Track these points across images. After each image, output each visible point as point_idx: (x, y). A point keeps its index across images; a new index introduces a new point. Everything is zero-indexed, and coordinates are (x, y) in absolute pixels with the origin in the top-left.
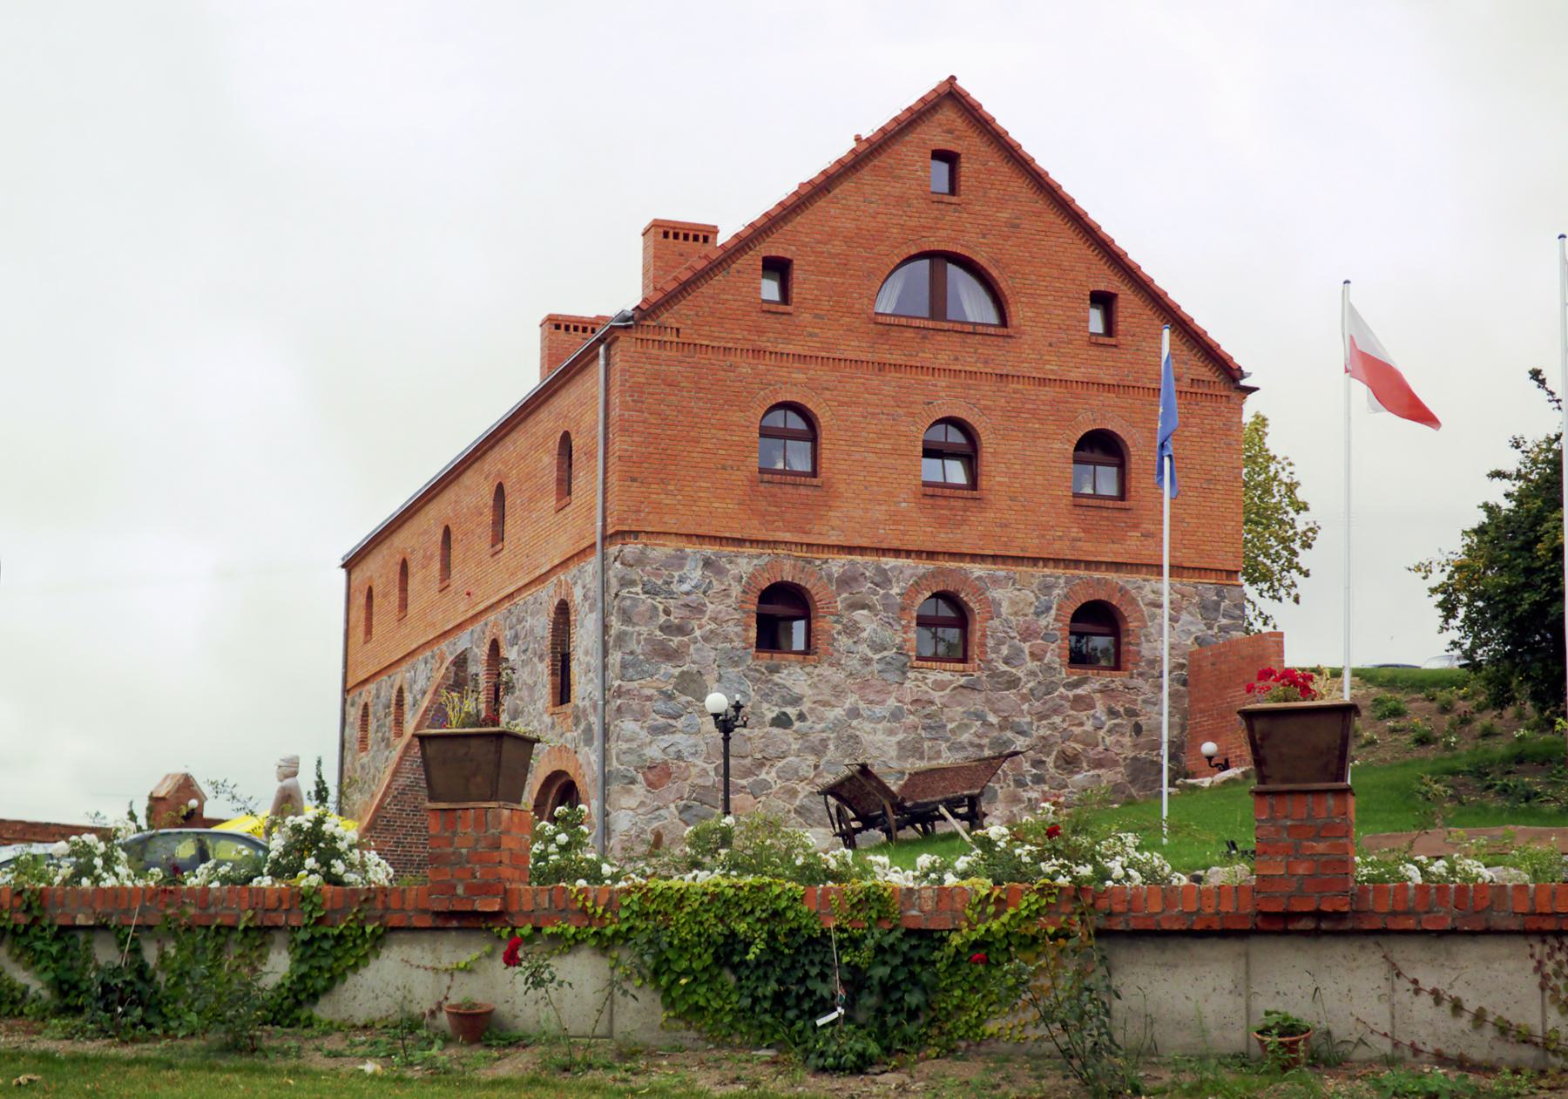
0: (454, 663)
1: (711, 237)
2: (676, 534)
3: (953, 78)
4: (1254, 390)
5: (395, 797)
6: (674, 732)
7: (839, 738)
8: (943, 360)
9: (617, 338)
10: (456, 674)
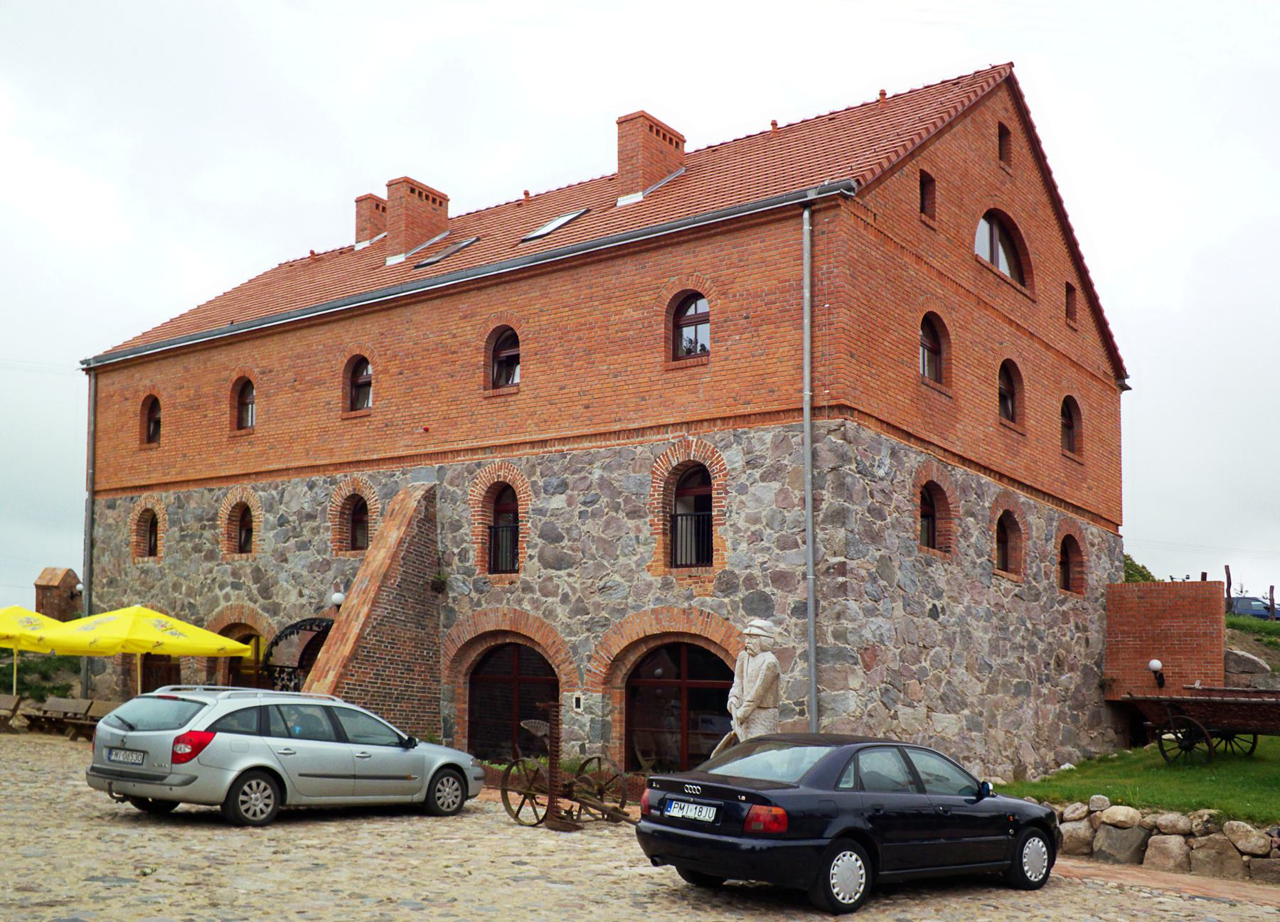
0: (425, 497)
1: (680, 144)
2: (876, 418)
3: (1011, 65)
4: (1129, 388)
5: (374, 627)
6: (877, 616)
7: (961, 632)
8: (1005, 308)
9: (839, 206)
10: (426, 509)
